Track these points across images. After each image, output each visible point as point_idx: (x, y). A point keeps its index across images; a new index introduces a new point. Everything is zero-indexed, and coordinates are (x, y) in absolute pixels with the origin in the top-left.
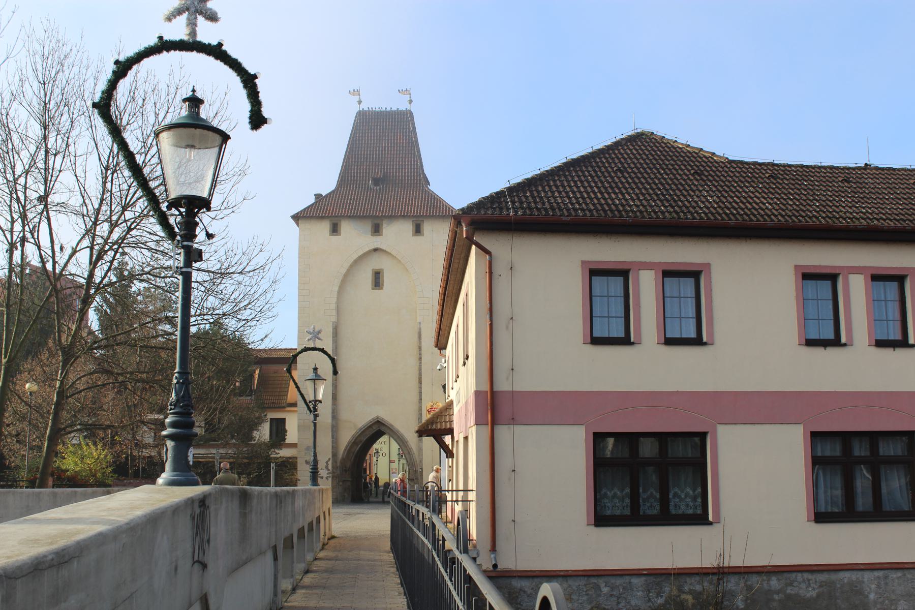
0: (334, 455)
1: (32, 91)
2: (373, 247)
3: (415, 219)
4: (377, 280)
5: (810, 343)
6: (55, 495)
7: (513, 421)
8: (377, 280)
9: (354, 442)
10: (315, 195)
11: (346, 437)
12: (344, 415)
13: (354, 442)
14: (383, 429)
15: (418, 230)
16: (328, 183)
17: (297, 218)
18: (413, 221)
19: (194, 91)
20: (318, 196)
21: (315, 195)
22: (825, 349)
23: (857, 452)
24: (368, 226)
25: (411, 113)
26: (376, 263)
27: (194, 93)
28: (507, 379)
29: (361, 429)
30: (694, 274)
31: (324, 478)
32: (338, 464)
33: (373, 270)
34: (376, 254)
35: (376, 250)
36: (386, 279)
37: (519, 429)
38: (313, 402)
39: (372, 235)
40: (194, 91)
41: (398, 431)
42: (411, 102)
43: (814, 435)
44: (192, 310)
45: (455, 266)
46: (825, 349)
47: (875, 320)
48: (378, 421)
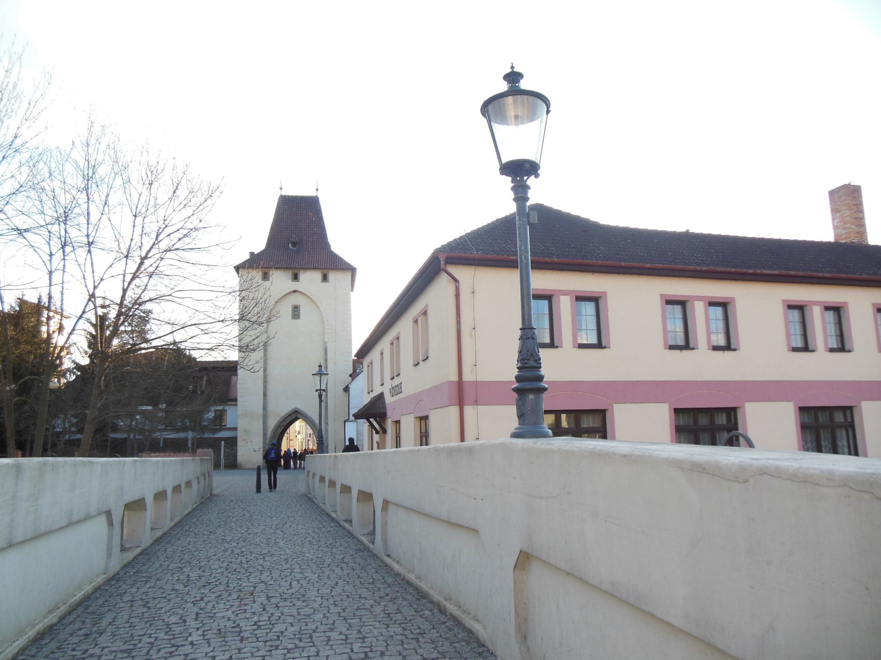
0: (265, 435)
1: (78, 156)
2: (293, 290)
3: (323, 271)
4: (296, 312)
5: (672, 347)
6: (18, 469)
7: (476, 402)
8: (296, 312)
9: (279, 425)
10: (250, 253)
11: (273, 423)
12: (271, 407)
13: (278, 426)
14: (299, 416)
15: (325, 278)
16: (259, 244)
17: (237, 268)
18: (321, 272)
19: (512, 68)
20: (252, 254)
21: (250, 253)
22: (681, 352)
23: (725, 422)
24: (289, 275)
25: (318, 198)
26: (295, 300)
27: (513, 70)
28: (472, 372)
29: (284, 416)
30: (595, 299)
31: (257, 451)
32: (267, 442)
33: (293, 305)
34: (295, 295)
35: (295, 291)
36: (303, 311)
37: (481, 408)
38: (319, 391)
39: (292, 281)
40: (512, 68)
41: (311, 418)
42: (317, 190)
43: (677, 411)
44: (57, 350)
45: (524, 276)
46: (681, 352)
47: (328, 374)
48: (296, 411)
